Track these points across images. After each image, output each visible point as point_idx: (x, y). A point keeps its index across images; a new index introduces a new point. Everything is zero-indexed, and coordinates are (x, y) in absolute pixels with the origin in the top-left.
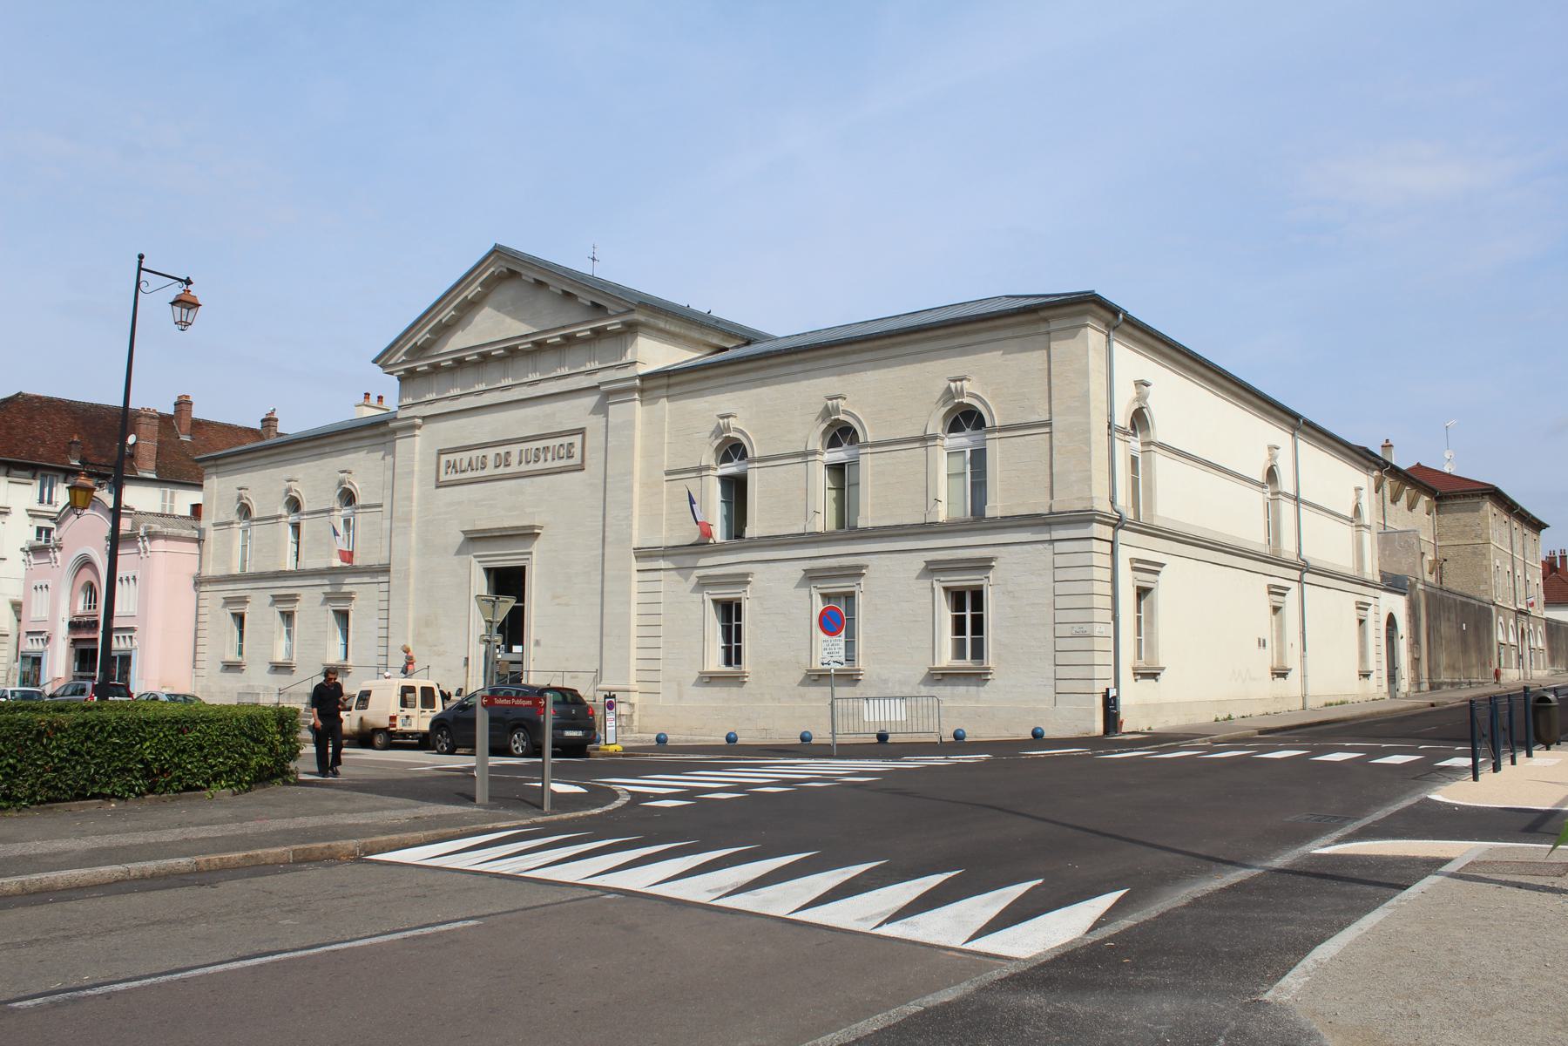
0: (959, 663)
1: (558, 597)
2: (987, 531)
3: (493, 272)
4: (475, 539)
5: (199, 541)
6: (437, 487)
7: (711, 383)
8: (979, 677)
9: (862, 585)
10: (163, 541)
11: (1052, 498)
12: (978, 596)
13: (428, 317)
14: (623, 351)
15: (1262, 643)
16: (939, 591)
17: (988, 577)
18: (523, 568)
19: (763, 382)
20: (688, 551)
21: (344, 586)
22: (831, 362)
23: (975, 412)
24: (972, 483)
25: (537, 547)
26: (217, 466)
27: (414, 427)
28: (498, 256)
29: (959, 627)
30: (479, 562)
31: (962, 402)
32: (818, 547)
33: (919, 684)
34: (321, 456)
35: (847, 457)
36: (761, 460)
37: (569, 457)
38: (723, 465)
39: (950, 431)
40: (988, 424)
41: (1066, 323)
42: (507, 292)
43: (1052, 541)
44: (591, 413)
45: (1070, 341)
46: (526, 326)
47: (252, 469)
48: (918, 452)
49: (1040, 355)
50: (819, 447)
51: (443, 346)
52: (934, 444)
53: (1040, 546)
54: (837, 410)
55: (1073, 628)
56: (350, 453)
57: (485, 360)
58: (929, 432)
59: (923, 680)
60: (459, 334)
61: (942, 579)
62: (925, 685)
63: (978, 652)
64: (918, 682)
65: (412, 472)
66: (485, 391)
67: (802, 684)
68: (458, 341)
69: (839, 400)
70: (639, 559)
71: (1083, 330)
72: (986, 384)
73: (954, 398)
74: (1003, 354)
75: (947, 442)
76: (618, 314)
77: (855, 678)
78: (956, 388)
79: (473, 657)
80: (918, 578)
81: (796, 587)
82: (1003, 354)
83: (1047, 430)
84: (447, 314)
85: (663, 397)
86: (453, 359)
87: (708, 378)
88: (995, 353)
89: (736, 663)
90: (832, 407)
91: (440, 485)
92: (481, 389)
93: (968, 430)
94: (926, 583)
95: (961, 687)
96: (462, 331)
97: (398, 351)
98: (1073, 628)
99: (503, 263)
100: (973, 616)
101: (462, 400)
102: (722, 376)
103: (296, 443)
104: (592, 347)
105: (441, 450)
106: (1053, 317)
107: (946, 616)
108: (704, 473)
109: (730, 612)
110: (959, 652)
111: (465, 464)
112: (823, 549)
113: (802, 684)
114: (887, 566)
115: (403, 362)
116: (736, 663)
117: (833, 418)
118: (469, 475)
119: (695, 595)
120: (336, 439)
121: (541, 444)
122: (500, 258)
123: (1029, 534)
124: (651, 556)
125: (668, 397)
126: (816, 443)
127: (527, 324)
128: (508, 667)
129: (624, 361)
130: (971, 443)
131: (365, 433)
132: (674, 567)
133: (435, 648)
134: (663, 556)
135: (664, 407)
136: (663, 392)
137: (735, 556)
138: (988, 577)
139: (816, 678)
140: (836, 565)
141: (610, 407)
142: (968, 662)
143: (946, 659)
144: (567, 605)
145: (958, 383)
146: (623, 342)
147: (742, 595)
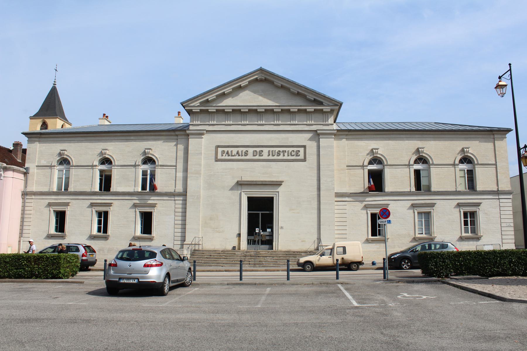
0: (99, 234)
1: (293, 210)
2: (478, 195)
3: (257, 78)
4: (240, 184)
5: (26, 174)
6: (216, 161)
7: (366, 136)
8: (106, 238)
9: (155, 209)
10: (12, 172)
11: (175, 187)
12: (106, 214)
13: (219, 89)
14: (327, 120)
15: (282, 228)
16: (94, 212)
17: (110, 208)
18: (272, 199)
19: (389, 139)
20: (360, 195)
21: (150, 201)
22: (417, 136)
23: (152, 160)
24: (468, 180)
25: (281, 189)
26: (40, 137)
27: (203, 134)
28: (261, 72)
29: (99, 222)
30: (245, 194)
31: (64, 157)
32: (417, 196)
33: (456, 241)
34: (127, 140)
35: (422, 168)
36: (161, 166)
37: (297, 156)
38: (59, 166)
39: (143, 164)
40: (71, 164)
41: (499, 136)
42: (261, 87)
43: (499, 199)
44: (308, 140)
45: (501, 141)
46: (271, 102)
47: (70, 142)
48: (133, 169)
49: (490, 145)
50: (56, 164)
51: (221, 102)
52: (458, 167)
53: (495, 200)
54: (105, 154)
55: (507, 224)
56: (149, 141)
57: (237, 112)
58: (137, 164)
59: (458, 239)
60: (230, 99)
61: (53, 208)
62: (458, 241)
63: (105, 231)
64: (456, 240)
65: (201, 153)
66: (248, 124)
67: (45, 238)
68: (229, 102)
69: (65, 151)
70: (336, 197)
71: (505, 139)
72: (474, 150)
73: (103, 155)
74: (479, 142)
75: (58, 168)
76: (329, 106)
77: (152, 239)
78: (147, 152)
79: (243, 233)
80: (454, 208)
81: (407, 209)
82: (479, 142)
83: (175, 168)
84: (227, 90)
85: (345, 139)
86: (216, 109)
87: (365, 134)
88: (477, 142)
89: (379, 235)
90: (147, 152)
91: (217, 160)
92: (232, 124)
93: (106, 165)
94: (90, 209)
95: (471, 242)
96: (232, 98)
97: (196, 101)
98: (507, 224)
99: (263, 75)
100: (470, 220)
101: (281, 126)
102: (371, 134)
103: (45, 134)
104: (229, 116)
105: (218, 146)
106: (496, 134)
107: (96, 219)
108: (94, 167)
109: (61, 217)
110: (99, 230)
111: (286, 154)
112: (419, 197)
113: (45, 238)
114: (443, 204)
115: (198, 106)
116: (379, 235)
117: (104, 156)
118: (237, 157)
119: (363, 211)
120: (141, 134)
121: (281, 149)
122: (262, 73)
123: (168, 198)
124: (342, 196)
125: (346, 139)
126: (96, 163)
127: (272, 101)
128: (265, 238)
129: (327, 123)
130: (467, 168)
131: (164, 133)
132: (138, 199)
133: (218, 229)
134: (34, 194)
135: (344, 142)
136: (344, 136)
137: (50, 197)
138: (110, 208)
139: (137, 238)
140: (424, 203)
141: (189, 139)
142: (470, 234)
143: (95, 232)
144: (298, 213)
145: (148, 150)
146: (197, 117)
147: (66, 209)
